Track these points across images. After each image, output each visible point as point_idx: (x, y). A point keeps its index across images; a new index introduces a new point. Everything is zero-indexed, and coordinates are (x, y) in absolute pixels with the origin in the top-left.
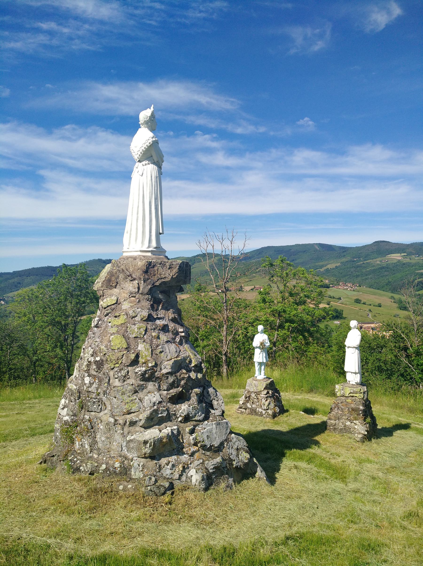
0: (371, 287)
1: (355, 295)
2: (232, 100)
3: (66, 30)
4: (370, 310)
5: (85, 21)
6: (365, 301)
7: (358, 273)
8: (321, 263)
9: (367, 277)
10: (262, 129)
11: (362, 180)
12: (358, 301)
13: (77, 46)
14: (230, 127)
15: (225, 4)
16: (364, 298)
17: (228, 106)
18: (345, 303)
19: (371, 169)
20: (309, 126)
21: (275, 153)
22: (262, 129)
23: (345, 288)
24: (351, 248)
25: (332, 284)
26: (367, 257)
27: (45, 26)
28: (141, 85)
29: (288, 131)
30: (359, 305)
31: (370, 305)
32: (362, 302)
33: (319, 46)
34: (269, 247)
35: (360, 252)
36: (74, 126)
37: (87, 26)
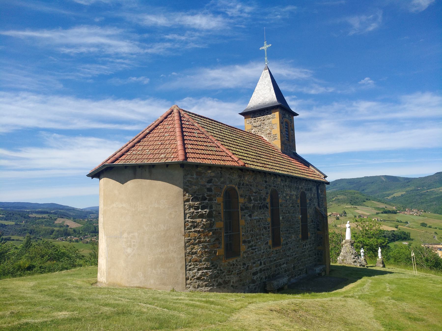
0: (436, 212)
1: (421, 220)
2: (305, 70)
3: (183, 38)
4: (436, 233)
5: (195, 30)
6: (430, 225)
7: (422, 200)
8: (387, 192)
9: (432, 203)
10: (331, 90)
11: (418, 122)
12: (424, 225)
13: (192, 46)
14: (305, 90)
15: (295, 8)
16: (430, 222)
17: (304, 76)
18: (412, 226)
19: (426, 112)
20: (369, 83)
21: (336, 106)
22: (331, 90)
23: (411, 213)
24: (415, 178)
25: (399, 210)
26: (429, 186)
27: (169, 37)
28: (237, 67)
29: (353, 89)
30: (424, 229)
31: (436, 228)
32: (428, 226)
33: (373, 27)
34: (341, 180)
35: (423, 182)
36: (191, 99)
37: (197, 34)
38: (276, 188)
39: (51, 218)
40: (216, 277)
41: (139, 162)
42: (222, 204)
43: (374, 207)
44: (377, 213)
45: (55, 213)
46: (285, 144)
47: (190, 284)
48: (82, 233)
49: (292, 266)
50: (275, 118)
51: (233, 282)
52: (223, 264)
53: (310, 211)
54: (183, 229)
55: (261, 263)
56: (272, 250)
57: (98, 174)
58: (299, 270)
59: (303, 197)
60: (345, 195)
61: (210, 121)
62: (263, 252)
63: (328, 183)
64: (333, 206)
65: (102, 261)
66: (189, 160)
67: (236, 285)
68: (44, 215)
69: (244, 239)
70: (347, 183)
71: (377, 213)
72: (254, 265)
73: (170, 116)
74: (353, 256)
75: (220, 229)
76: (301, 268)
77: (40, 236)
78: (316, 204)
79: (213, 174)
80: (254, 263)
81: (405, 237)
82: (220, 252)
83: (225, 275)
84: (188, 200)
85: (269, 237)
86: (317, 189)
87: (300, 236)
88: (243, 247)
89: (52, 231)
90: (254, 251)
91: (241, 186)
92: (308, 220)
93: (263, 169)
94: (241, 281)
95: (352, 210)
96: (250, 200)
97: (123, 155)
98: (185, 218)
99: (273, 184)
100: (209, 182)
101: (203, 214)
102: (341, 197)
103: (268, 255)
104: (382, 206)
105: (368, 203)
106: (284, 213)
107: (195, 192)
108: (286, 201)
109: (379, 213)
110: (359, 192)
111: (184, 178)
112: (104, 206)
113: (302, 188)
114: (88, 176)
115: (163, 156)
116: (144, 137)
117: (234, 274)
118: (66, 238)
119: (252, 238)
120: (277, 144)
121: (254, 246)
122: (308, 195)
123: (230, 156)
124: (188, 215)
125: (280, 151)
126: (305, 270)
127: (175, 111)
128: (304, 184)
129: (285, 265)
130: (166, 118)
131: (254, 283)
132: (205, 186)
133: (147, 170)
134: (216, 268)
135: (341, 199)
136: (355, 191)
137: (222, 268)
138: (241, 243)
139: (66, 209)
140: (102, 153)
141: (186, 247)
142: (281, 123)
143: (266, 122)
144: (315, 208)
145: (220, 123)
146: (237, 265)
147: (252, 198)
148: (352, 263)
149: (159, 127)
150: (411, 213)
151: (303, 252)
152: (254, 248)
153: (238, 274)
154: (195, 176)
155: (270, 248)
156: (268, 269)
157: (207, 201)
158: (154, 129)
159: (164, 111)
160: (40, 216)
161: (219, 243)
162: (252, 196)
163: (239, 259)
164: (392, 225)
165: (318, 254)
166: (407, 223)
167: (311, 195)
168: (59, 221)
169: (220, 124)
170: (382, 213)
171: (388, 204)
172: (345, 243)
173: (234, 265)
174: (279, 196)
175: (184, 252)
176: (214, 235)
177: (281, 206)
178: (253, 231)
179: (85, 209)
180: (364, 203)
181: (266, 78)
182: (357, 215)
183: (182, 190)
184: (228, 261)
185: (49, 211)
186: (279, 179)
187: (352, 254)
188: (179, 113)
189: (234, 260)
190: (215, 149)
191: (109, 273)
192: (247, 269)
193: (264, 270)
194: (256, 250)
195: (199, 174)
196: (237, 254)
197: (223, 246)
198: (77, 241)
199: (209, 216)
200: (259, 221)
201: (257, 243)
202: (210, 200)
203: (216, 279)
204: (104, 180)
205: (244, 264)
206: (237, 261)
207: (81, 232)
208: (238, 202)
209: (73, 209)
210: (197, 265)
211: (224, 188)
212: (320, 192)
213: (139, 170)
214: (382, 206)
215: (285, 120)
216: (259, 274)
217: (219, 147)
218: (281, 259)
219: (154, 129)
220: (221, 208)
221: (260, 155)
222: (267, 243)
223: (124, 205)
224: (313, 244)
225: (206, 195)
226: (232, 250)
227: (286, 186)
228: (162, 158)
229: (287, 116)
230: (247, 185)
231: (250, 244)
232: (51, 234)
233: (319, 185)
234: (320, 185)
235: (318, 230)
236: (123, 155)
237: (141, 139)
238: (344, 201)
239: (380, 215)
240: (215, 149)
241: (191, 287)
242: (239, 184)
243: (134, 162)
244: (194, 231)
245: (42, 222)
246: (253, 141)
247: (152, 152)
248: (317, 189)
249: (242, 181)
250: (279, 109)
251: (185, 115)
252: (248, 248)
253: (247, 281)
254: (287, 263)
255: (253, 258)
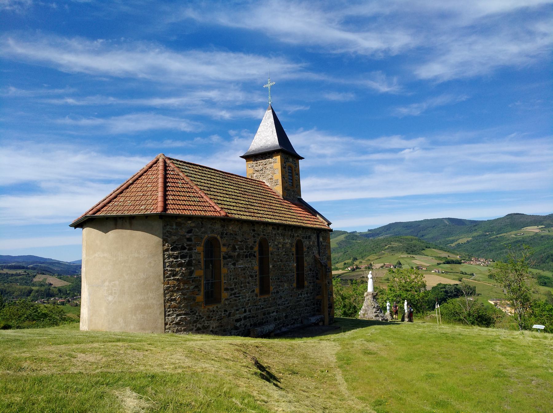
8: (451, 238)
18: (478, 279)
23: (478, 263)
26: (500, 231)
34: (396, 224)
35: (492, 226)
38: (266, 237)
39: (28, 274)
40: (195, 322)
41: (119, 214)
42: (202, 253)
43: (435, 257)
44: (438, 264)
45: (33, 268)
46: (288, 190)
47: (169, 328)
48: (69, 293)
49: (284, 315)
50: (276, 162)
51: (213, 328)
52: (202, 310)
53: (308, 260)
54: (162, 277)
55: (245, 311)
56: (258, 298)
57: (81, 224)
58: (293, 319)
59: (299, 246)
60: (401, 242)
61: (200, 168)
62: (249, 300)
63: (331, 230)
64: (386, 255)
65: (84, 311)
66: (170, 212)
67: (216, 330)
68: (19, 271)
69: (225, 287)
70: (403, 227)
71: (438, 264)
72: (238, 312)
73: (155, 165)
74: (374, 310)
75: (200, 277)
76: (295, 317)
77: (13, 298)
78: (316, 252)
79: (193, 225)
80: (237, 310)
81: (471, 292)
82: (200, 297)
83: (204, 321)
84: (167, 250)
85: (256, 285)
86: (318, 237)
87: (295, 285)
88: (225, 295)
89: (30, 292)
90: (238, 298)
91: (224, 235)
92: (305, 268)
93: (251, 218)
94: (222, 326)
95: (408, 260)
96: (234, 249)
97: (105, 206)
98: (164, 267)
99: (263, 232)
100: (189, 232)
101: (182, 263)
102: (395, 244)
103: (255, 303)
104: (444, 254)
105: (427, 251)
106: (275, 261)
107: (174, 242)
108: (278, 249)
109: (440, 264)
110: (417, 238)
111: (163, 229)
112: (86, 256)
113: (298, 236)
114: (71, 226)
115: (143, 207)
116: (127, 188)
117: (214, 320)
118: (48, 300)
119: (235, 285)
120: (279, 189)
121: (239, 294)
122: (306, 243)
123: (213, 207)
124: (167, 264)
125: (281, 197)
126: (300, 319)
127: (161, 160)
128: (300, 232)
129: (275, 313)
130: (151, 167)
131: (237, 330)
132: (185, 236)
133: (128, 221)
134: (195, 314)
135: (396, 247)
136: (412, 237)
137: (201, 314)
138: (223, 290)
139: (48, 263)
140: (86, 203)
141: (165, 295)
142: (283, 167)
143: (268, 166)
144: (314, 256)
145: (212, 169)
146: (217, 312)
147: (237, 247)
148: (374, 318)
149: (143, 177)
150: (478, 263)
151: (298, 301)
152: (237, 295)
153: (218, 320)
154: (174, 227)
155: (257, 295)
156: (253, 317)
157: (186, 251)
158: (137, 179)
159: (147, 161)
160: (14, 272)
161: (199, 290)
162: (238, 245)
163: (219, 306)
164: (455, 277)
165: (317, 304)
166: (472, 275)
167: (310, 243)
168: (39, 278)
169: (213, 171)
170: (444, 263)
171: (451, 252)
172: (367, 295)
173: (214, 311)
174: (269, 244)
175: (163, 298)
176: (193, 283)
177: (271, 254)
178: (236, 279)
179: (74, 263)
180: (423, 251)
181: (268, 118)
182: (414, 267)
183: (161, 240)
184: (207, 307)
185: (25, 266)
186: (270, 228)
187: (374, 307)
188: (165, 162)
189: (215, 306)
190: (198, 199)
191: (90, 321)
192: (229, 315)
193: (249, 317)
194: (240, 297)
195: (179, 225)
196: (218, 300)
197: (202, 293)
198: (63, 304)
199: (189, 264)
200: (244, 269)
201: (241, 291)
202: (190, 249)
203: (195, 324)
204: (87, 231)
205: (226, 311)
206: (217, 307)
207: (68, 292)
208: (220, 252)
209: (59, 263)
210: (176, 311)
211: (205, 238)
212: (321, 239)
213: (120, 222)
214: (444, 254)
215: (288, 164)
216: (243, 322)
217: (202, 198)
218: (270, 307)
219: (137, 179)
220: (202, 257)
221: (251, 204)
222: (254, 291)
223: (105, 255)
224: (311, 293)
225: (185, 245)
226: (212, 297)
227: (278, 234)
228: (142, 210)
229: (291, 160)
230: (231, 234)
231: (233, 292)
232: (28, 296)
233: (320, 232)
234: (324, 233)
235: (317, 279)
236: (105, 206)
237: (123, 190)
238: (398, 250)
239: (441, 265)
240: (198, 199)
241: (170, 331)
242: (222, 234)
243: (114, 214)
244: (173, 279)
245: (17, 280)
246: (255, 186)
247: (133, 203)
248: (318, 237)
249: (226, 230)
250: (280, 153)
251: (171, 165)
252: (231, 295)
253: (229, 327)
254: (277, 312)
255: (237, 306)
